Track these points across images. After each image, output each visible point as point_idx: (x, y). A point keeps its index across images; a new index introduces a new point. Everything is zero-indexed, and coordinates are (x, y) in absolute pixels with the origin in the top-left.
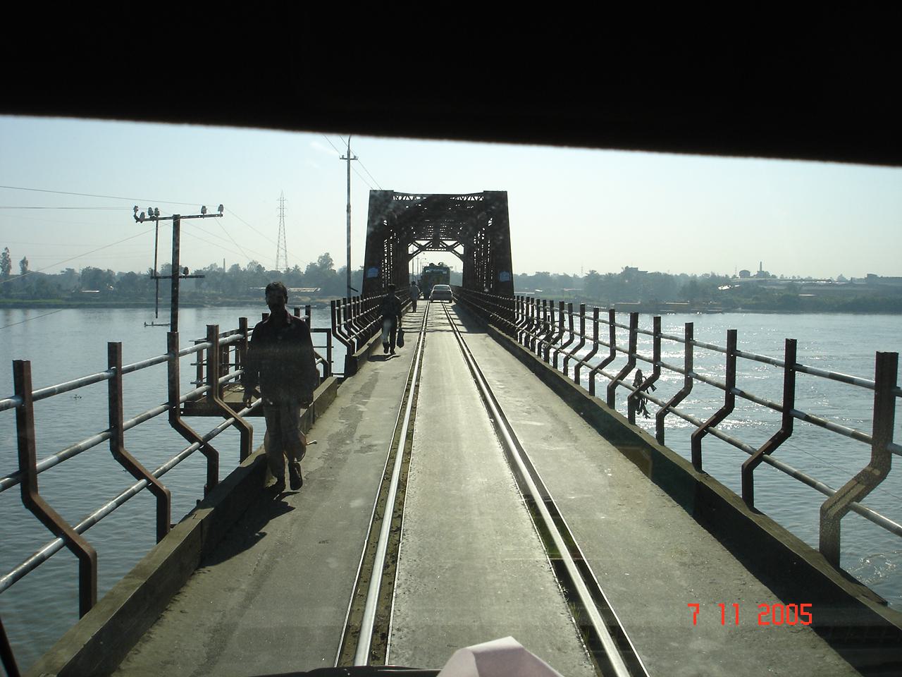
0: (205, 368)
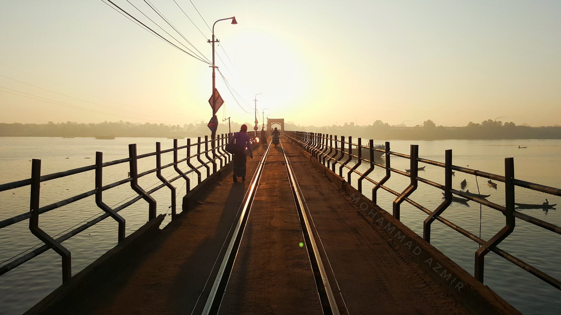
0: (228, 139)
